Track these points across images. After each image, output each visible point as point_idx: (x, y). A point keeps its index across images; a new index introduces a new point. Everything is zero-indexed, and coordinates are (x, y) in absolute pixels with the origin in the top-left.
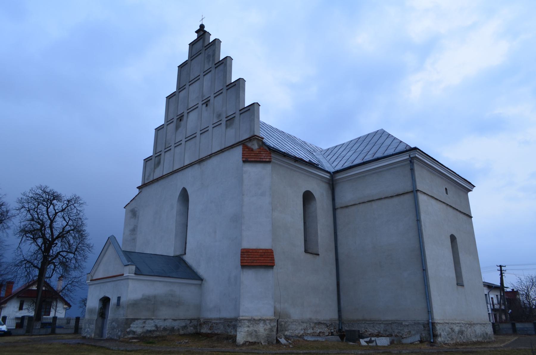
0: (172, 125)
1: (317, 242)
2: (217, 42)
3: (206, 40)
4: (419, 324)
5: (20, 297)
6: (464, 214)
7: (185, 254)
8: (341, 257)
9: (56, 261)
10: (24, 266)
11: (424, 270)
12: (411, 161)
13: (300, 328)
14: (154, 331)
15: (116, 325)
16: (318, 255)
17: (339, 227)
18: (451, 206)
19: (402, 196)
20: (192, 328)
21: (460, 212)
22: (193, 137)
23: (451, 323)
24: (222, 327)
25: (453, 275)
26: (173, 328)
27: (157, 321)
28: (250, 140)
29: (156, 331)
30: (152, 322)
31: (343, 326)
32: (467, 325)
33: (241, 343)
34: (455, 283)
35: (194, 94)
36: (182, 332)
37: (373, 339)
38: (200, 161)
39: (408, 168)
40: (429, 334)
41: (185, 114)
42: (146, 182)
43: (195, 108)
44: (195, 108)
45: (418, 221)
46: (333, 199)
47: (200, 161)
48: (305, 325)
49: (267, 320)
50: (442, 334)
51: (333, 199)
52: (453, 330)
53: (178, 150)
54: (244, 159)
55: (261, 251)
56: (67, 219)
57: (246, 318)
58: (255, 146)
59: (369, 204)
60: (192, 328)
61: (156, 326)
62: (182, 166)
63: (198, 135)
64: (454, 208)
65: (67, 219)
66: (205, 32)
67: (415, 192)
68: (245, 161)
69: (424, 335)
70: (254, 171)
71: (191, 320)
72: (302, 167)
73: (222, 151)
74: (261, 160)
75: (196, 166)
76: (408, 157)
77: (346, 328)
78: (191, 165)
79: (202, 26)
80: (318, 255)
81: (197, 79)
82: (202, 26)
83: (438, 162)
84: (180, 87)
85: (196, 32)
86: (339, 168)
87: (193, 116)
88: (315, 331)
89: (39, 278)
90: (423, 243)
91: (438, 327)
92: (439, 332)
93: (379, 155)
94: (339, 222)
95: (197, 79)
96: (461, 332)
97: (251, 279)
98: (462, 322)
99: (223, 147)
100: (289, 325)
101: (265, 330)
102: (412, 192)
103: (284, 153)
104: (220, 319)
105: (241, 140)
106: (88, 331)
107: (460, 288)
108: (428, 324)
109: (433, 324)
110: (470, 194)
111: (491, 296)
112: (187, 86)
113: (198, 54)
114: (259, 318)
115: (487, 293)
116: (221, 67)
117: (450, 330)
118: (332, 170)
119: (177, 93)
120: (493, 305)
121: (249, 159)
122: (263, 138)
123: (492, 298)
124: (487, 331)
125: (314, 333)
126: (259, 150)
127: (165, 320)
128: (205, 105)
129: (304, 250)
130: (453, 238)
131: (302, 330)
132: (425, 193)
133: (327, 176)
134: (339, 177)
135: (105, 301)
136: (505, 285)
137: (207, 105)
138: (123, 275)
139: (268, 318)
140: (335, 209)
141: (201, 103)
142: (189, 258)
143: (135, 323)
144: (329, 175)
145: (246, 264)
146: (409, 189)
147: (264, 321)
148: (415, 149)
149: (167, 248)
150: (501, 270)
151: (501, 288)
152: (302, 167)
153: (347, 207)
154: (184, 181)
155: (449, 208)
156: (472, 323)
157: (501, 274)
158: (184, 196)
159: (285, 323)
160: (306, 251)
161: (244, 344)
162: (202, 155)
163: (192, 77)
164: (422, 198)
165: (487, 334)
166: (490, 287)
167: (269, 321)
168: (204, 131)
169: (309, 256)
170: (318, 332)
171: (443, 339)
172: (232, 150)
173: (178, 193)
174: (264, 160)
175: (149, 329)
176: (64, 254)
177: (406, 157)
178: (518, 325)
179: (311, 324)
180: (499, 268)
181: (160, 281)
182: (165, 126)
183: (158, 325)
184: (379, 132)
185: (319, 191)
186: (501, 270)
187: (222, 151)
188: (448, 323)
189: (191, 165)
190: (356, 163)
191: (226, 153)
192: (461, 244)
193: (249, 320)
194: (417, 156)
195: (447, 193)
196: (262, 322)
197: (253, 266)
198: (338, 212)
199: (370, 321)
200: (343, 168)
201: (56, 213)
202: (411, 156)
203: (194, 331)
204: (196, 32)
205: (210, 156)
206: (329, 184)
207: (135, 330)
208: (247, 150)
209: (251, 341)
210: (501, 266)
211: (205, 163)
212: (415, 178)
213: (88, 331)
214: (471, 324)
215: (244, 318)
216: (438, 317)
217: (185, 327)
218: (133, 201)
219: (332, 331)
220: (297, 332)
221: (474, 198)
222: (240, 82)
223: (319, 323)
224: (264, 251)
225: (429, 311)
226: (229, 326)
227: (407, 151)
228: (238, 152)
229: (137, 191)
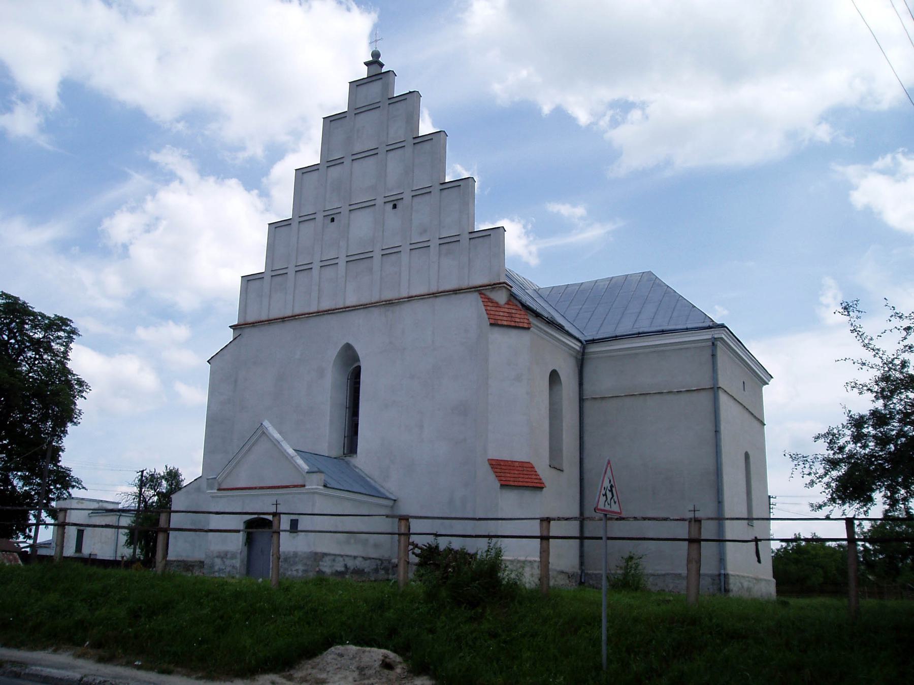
1: (561, 450)
12: (714, 342)
17: (587, 428)
19: (695, 394)
22: (365, 257)
30: (341, 559)
39: (708, 353)
40: (720, 589)
42: (251, 319)
45: (717, 432)
46: (581, 384)
53: (329, 272)
54: (493, 321)
58: (501, 297)
59: (642, 398)
67: (715, 389)
69: (21, 538)
70: (505, 342)
72: (553, 333)
75: (375, 312)
76: (710, 337)
81: (373, 153)
90: (721, 464)
91: (731, 580)
92: (731, 586)
94: (587, 421)
99: (434, 289)
109: (726, 576)
110: (765, 388)
121: (499, 322)
128: (391, 205)
130: (747, 456)
137: (395, 207)
140: (581, 400)
144: (579, 344)
152: (553, 333)
164: (723, 398)
172: (453, 296)
174: (521, 325)
177: (707, 335)
198: (587, 405)
204: (367, 64)
208: (489, 304)
211: (397, 309)
216: (731, 569)
218: (225, 350)
221: (771, 395)
227: (710, 327)
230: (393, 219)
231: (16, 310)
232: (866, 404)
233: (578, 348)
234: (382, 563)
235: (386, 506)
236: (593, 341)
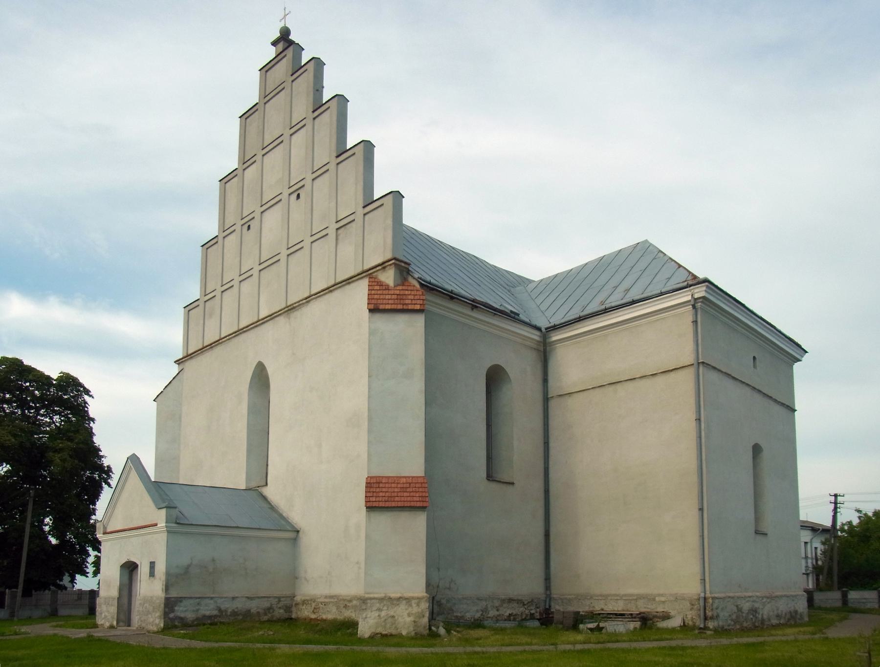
4: (684, 599)
6: (783, 404)
7: (267, 484)
13: (475, 608)
14: (216, 616)
15: (151, 608)
18: (760, 391)
19: (672, 374)
20: (282, 611)
21: (776, 401)
23: (738, 598)
24: (334, 609)
26: (249, 611)
27: (219, 601)
28: (384, 268)
29: (220, 617)
30: (212, 602)
31: (552, 604)
32: (765, 600)
33: (367, 636)
35: (273, 172)
36: (265, 618)
37: (601, 625)
38: (290, 309)
41: (257, 215)
42: (190, 352)
43: (276, 201)
44: (276, 201)
47: (290, 309)
48: (484, 603)
49: (413, 598)
50: (721, 614)
51: (545, 381)
52: (740, 610)
54: (372, 307)
55: (404, 480)
57: (376, 596)
60: (282, 611)
61: (220, 610)
62: (256, 319)
63: (283, 257)
64: (765, 395)
66: (291, 43)
71: (279, 599)
72: (491, 321)
73: (329, 290)
74: (405, 307)
75: (281, 320)
76: (689, 298)
77: (557, 607)
78: (271, 317)
81: (278, 141)
83: (743, 305)
84: (246, 161)
86: (556, 320)
87: (273, 219)
88: (501, 612)
93: (634, 294)
95: (278, 141)
96: (754, 611)
98: (758, 594)
100: (455, 604)
101: (409, 615)
103: (452, 292)
104: (331, 597)
105: (366, 267)
106: (106, 617)
108: (699, 599)
110: (796, 366)
112: (258, 158)
113: (279, 89)
114: (399, 595)
115: (808, 540)
117: (735, 609)
118: (543, 324)
119: (239, 172)
120: (817, 560)
121: (381, 307)
124: (797, 608)
125: (499, 615)
127: (233, 598)
128: (295, 196)
129: (485, 475)
130: (757, 450)
131: (477, 611)
132: (714, 368)
133: (535, 336)
134: (556, 337)
135: (130, 568)
137: (298, 196)
138: (156, 525)
139: (416, 595)
140: (546, 400)
141: (286, 192)
143: (182, 604)
144: (538, 333)
145: (375, 504)
147: (408, 600)
150: (836, 503)
152: (491, 321)
154: (265, 347)
155: (757, 396)
156: (774, 595)
157: (835, 510)
158: (261, 379)
159: (448, 601)
160: (490, 477)
161: (372, 637)
162: (293, 299)
163: (268, 139)
165: (796, 612)
166: (814, 529)
167: (416, 601)
168: (294, 250)
169: (493, 485)
170: (507, 614)
171: (721, 623)
172: (347, 287)
174: (410, 307)
175: (208, 613)
178: (853, 595)
179: (495, 601)
180: (833, 499)
181: (222, 535)
182: (220, 239)
183: (223, 607)
184: (639, 247)
185: (520, 369)
186: (836, 503)
187: (329, 290)
188: (733, 598)
189: (271, 317)
190: (588, 311)
191: (337, 294)
193: (381, 600)
195: (755, 366)
196: (404, 602)
197: (388, 507)
198: (552, 404)
199: (601, 595)
200: (563, 321)
202: (696, 296)
203: (286, 616)
205: (308, 299)
206: (538, 350)
207: (182, 615)
208: (377, 288)
209: (384, 633)
210: (836, 496)
211: (297, 314)
213: (106, 617)
214: (771, 598)
215: (372, 596)
217: (270, 609)
219: (532, 612)
220: (468, 615)
223: (511, 600)
224: (410, 480)
226: (346, 607)
229: (175, 369)
230: (298, 209)
231: (17, 368)
232: (870, 514)
233: (537, 338)
234: (280, 601)
235: (286, 539)
236: (555, 328)
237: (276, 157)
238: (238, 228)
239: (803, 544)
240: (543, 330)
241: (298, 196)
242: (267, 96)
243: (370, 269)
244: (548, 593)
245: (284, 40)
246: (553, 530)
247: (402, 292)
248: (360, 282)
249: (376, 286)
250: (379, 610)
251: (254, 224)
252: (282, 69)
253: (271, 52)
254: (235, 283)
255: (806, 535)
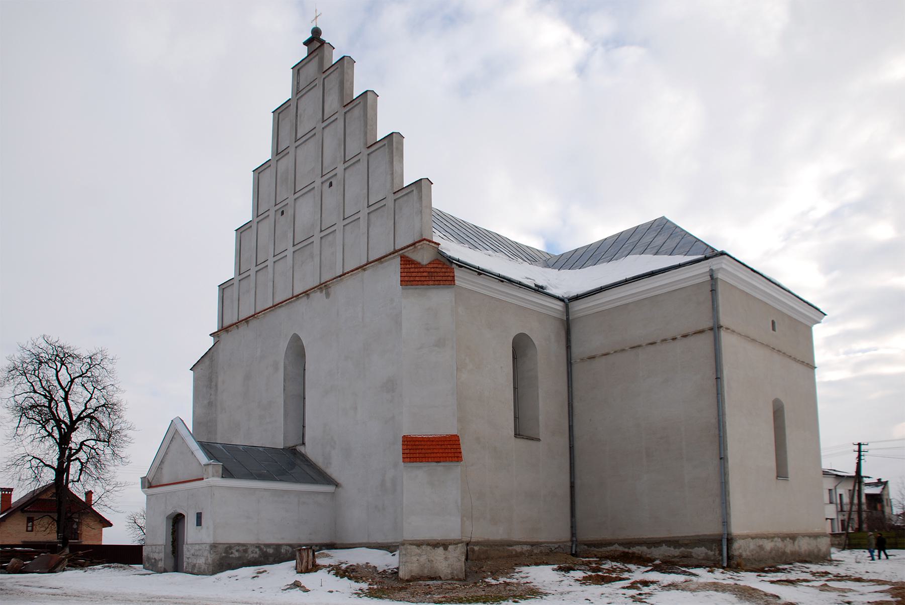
0: (266, 222)
2: (345, 63)
3: (325, 61)
5: (26, 511)
8: (577, 445)
9: (82, 455)
10: (28, 465)
11: (723, 459)
16: (539, 440)
21: (795, 359)
25: (772, 464)
34: (774, 474)
38: (323, 287)
46: (568, 347)
51: (568, 347)
56: (91, 388)
65: (91, 388)
66: (323, 42)
68: (404, 282)
79: (316, 32)
80: (539, 440)
82: (316, 32)
84: (278, 152)
85: (306, 43)
89: (57, 494)
90: (724, 414)
97: (419, 480)
102: (711, 329)
107: (781, 483)
111: (839, 491)
112: (292, 150)
116: (357, 112)
119: (273, 163)
122: (439, 244)
123: (841, 495)
126: (429, 271)
133: (559, 306)
134: (577, 306)
136: (863, 474)
137: (331, 185)
141: (319, 181)
142: (310, 450)
144: (561, 304)
146: (708, 324)
148: (723, 254)
149: (270, 434)
150: (859, 451)
151: (858, 478)
153: (592, 358)
154: (306, 320)
158: (297, 351)
160: (517, 435)
169: (521, 442)
173: (284, 345)
176: (92, 443)
180: (856, 448)
186: (859, 451)
192: (789, 420)
194: (724, 266)
195: (774, 329)
196: (441, 548)
201: (72, 381)
204: (306, 43)
210: (859, 444)
212: (717, 306)
222: (393, 141)
225: (726, 522)
228: (394, 268)
230: (331, 198)
237: (308, 152)
238: (272, 213)
239: (827, 491)
240: (566, 300)
241: (331, 185)
242: (298, 91)
243: (402, 249)
244: (271, 559)
245: (316, 42)
246: (578, 483)
247: (432, 270)
248: (394, 258)
249: (406, 262)
250: (420, 555)
251: (289, 212)
252: (312, 69)
253: (304, 52)
254: (270, 263)
255: (829, 483)
